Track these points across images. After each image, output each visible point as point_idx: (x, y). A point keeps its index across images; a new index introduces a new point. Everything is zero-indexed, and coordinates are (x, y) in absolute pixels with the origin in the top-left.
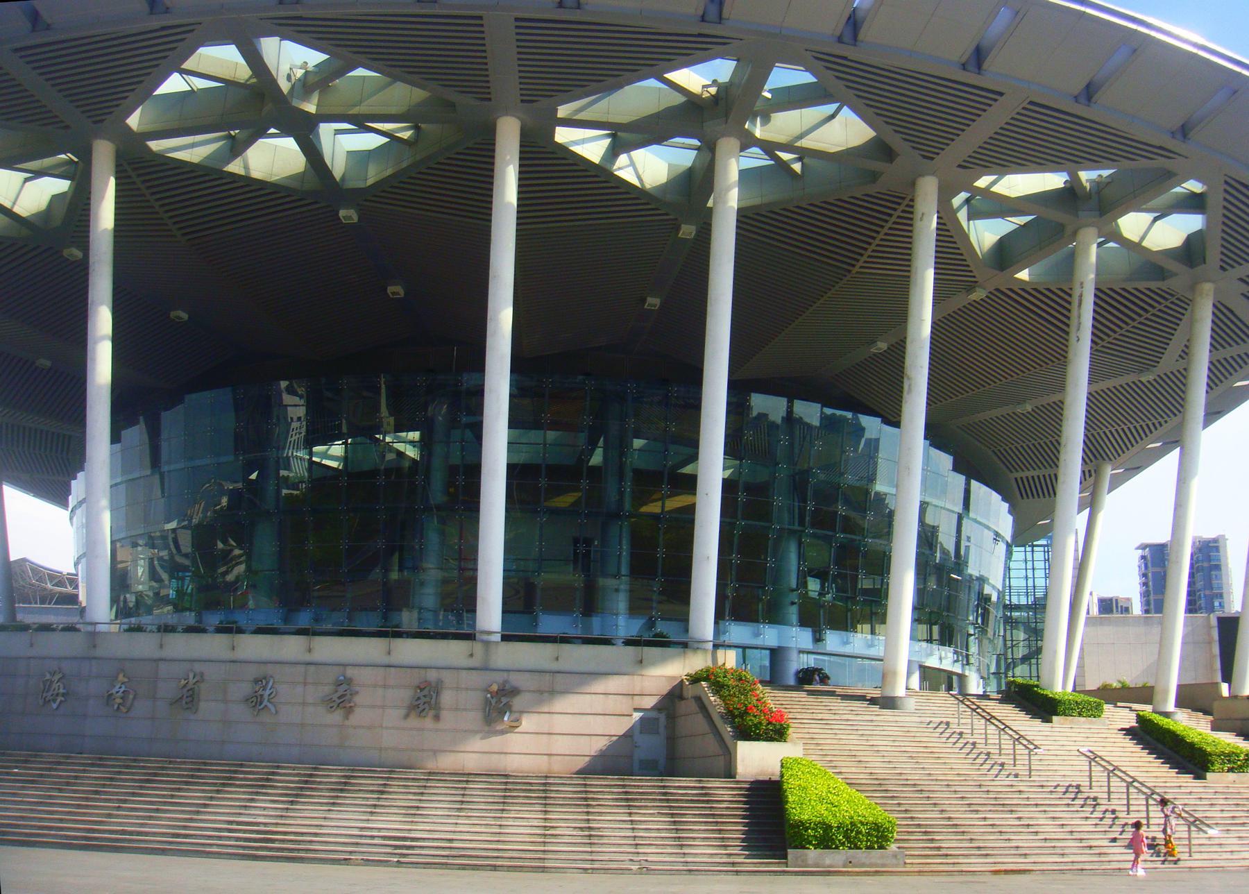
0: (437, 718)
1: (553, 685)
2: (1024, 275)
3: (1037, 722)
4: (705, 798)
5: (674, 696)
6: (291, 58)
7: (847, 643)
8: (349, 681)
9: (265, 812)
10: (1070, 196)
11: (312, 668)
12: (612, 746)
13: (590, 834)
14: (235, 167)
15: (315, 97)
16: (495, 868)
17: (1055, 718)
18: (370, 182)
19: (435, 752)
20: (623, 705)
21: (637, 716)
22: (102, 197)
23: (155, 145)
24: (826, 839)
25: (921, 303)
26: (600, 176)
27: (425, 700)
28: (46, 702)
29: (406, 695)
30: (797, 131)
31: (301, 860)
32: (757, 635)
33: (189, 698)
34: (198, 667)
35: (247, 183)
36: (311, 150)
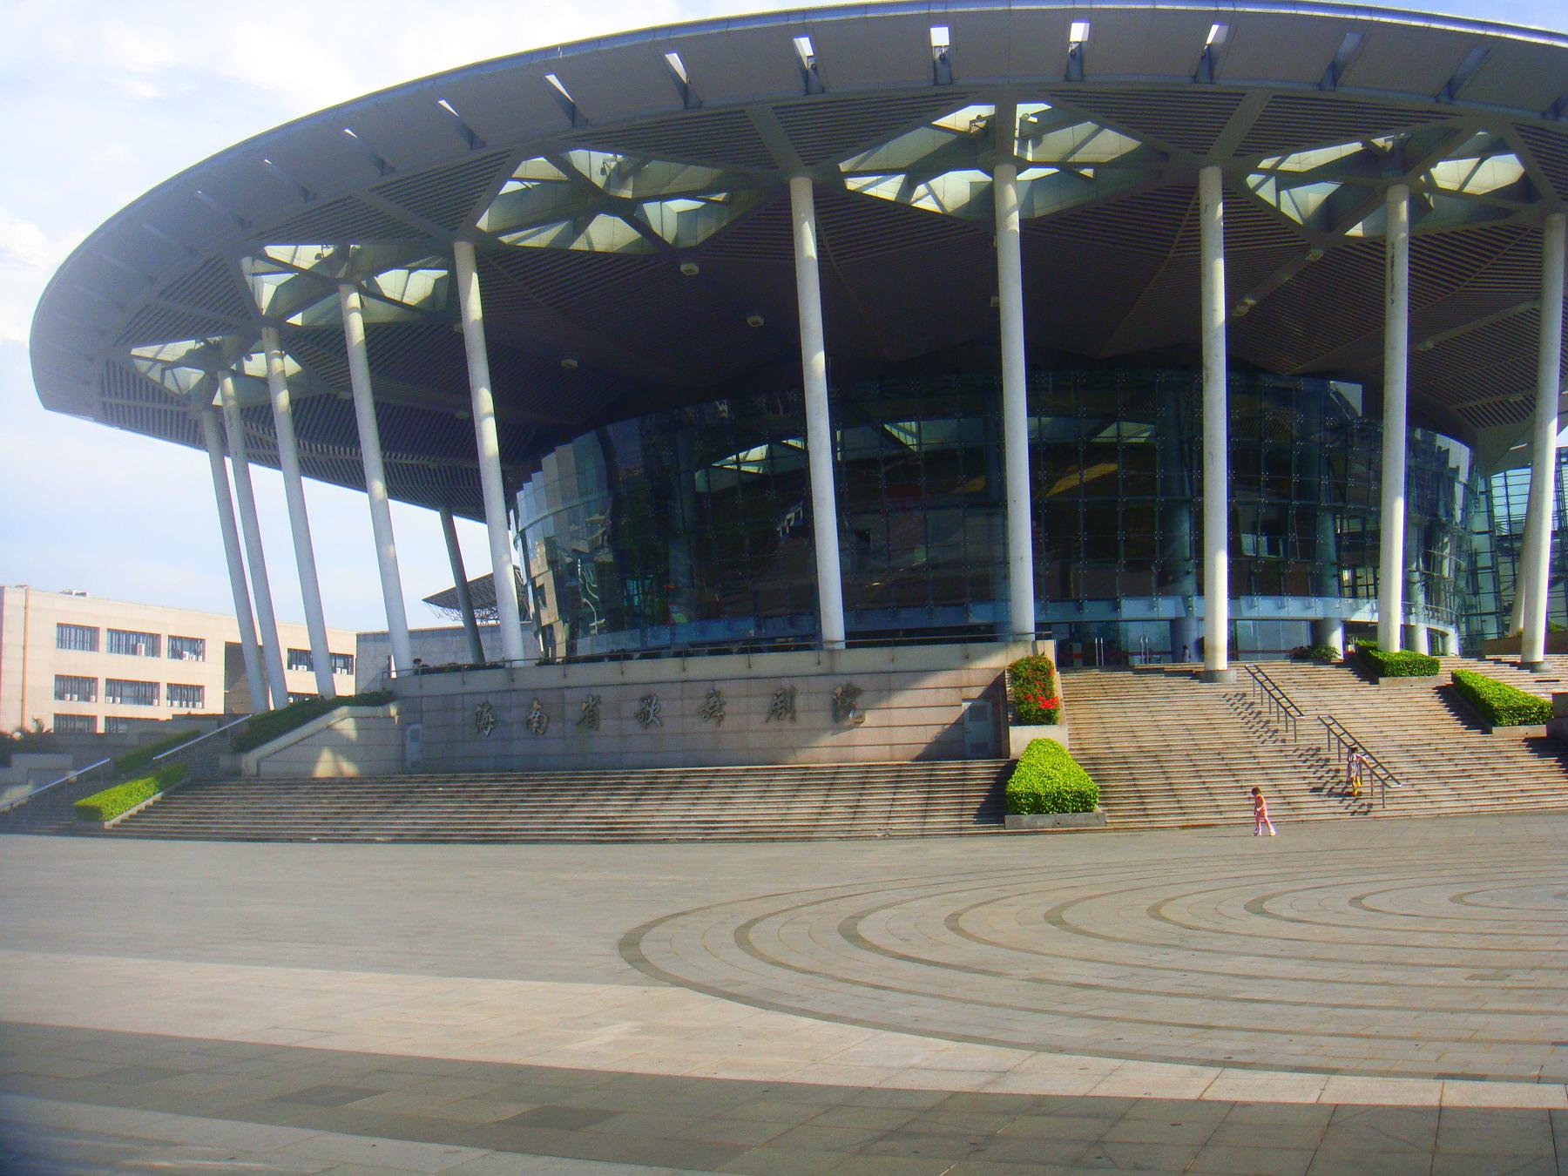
0: (793, 719)
1: (890, 684)
2: (1357, 231)
3: (1366, 684)
4: (964, 776)
5: (997, 686)
6: (594, 163)
7: (1281, 607)
8: (717, 694)
9: (614, 808)
10: (1370, 157)
11: (687, 685)
12: (944, 734)
13: (856, 810)
14: (579, 245)
15: (630, 182)
16: (773, 840)
17: (1381, 680)
18: (700, 240)
19: (794, 749)
20: (952, 697)
21: (966, 705)
22: (468, 292)
23: (505, 239)
24: (1037, 805)
25: (1212, 293)
26: (900, 209)
27: (783, 705)
28: (480, 730)
29: (765, 702)
30: (1070, 145)
31: (633, 841)
32: (1152, 607)
33: (590, 718)
34: (595, 692)
35: (592, 256)
36: (641, 224)
